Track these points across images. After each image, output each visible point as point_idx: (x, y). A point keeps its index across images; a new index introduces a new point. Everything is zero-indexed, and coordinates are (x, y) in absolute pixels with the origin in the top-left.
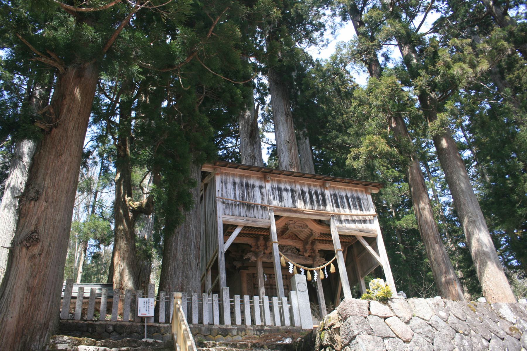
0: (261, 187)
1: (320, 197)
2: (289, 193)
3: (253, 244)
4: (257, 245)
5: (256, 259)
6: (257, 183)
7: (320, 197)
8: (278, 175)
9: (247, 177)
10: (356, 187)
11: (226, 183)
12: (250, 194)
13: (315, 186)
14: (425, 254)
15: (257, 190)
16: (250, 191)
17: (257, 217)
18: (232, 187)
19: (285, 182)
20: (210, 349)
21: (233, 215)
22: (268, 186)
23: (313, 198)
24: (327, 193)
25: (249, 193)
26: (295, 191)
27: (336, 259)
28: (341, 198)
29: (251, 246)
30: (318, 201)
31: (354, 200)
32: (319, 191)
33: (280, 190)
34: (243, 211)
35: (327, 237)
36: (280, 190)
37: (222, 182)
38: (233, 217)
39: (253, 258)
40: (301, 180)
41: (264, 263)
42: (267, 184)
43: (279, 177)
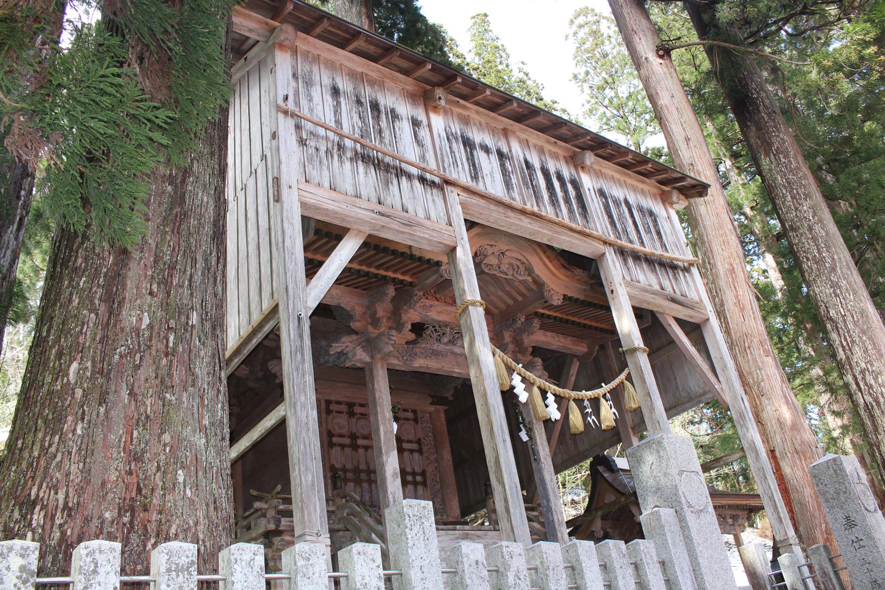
0: (416, 123)
1: (570, 187)
2: (494, 158)
3: (358, 311)
4: (370, 310)
5: (368, 359)
6: (404, 109)
7: (570, 187)
8: (462, 102)
9: (372, 83)
10: (643, 182)
11: (309, 84)
12: (386, 134)
13: (555, 156)
14: (526, 404)
15: (405, 127)
16: (384, 124)
17: (410, 209)
18: (328, 98)
19: (480, 127)
20: (19, 337)
21: (333, 188)
22: (438, 122)
23: (554, 189)
24: (587, 182)
25: (380, 132)
26: (510, 158)
27: (282, 424)
28: (617, 203)
29: (350, 316)
30: (567, 200)
31: (644, 215)
32: (566, 174)
33: (468, 144)
34: (367, 180)
35: (597, 302)
36: (468, 144)
37: (295, 76)
38: (334, 195)
39: (361, 356)
40: (523, 131)
41: (392, 373)
42: (433, 117)
43: (464, 107)
